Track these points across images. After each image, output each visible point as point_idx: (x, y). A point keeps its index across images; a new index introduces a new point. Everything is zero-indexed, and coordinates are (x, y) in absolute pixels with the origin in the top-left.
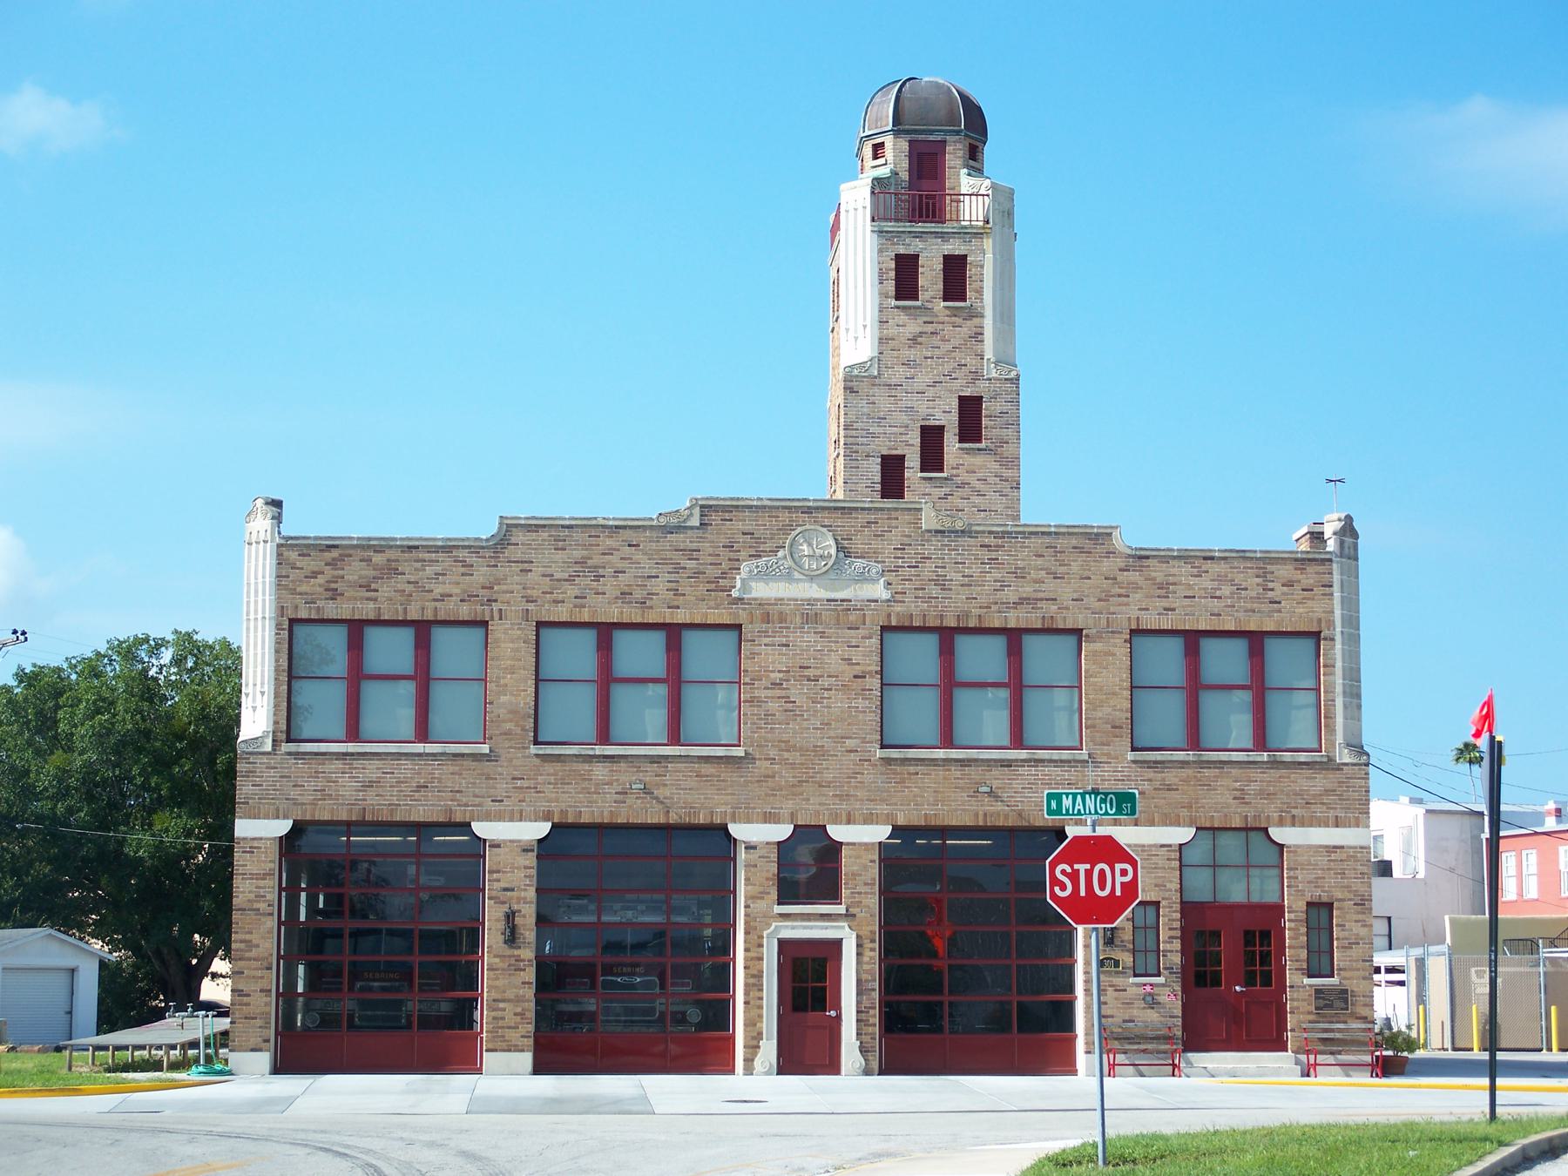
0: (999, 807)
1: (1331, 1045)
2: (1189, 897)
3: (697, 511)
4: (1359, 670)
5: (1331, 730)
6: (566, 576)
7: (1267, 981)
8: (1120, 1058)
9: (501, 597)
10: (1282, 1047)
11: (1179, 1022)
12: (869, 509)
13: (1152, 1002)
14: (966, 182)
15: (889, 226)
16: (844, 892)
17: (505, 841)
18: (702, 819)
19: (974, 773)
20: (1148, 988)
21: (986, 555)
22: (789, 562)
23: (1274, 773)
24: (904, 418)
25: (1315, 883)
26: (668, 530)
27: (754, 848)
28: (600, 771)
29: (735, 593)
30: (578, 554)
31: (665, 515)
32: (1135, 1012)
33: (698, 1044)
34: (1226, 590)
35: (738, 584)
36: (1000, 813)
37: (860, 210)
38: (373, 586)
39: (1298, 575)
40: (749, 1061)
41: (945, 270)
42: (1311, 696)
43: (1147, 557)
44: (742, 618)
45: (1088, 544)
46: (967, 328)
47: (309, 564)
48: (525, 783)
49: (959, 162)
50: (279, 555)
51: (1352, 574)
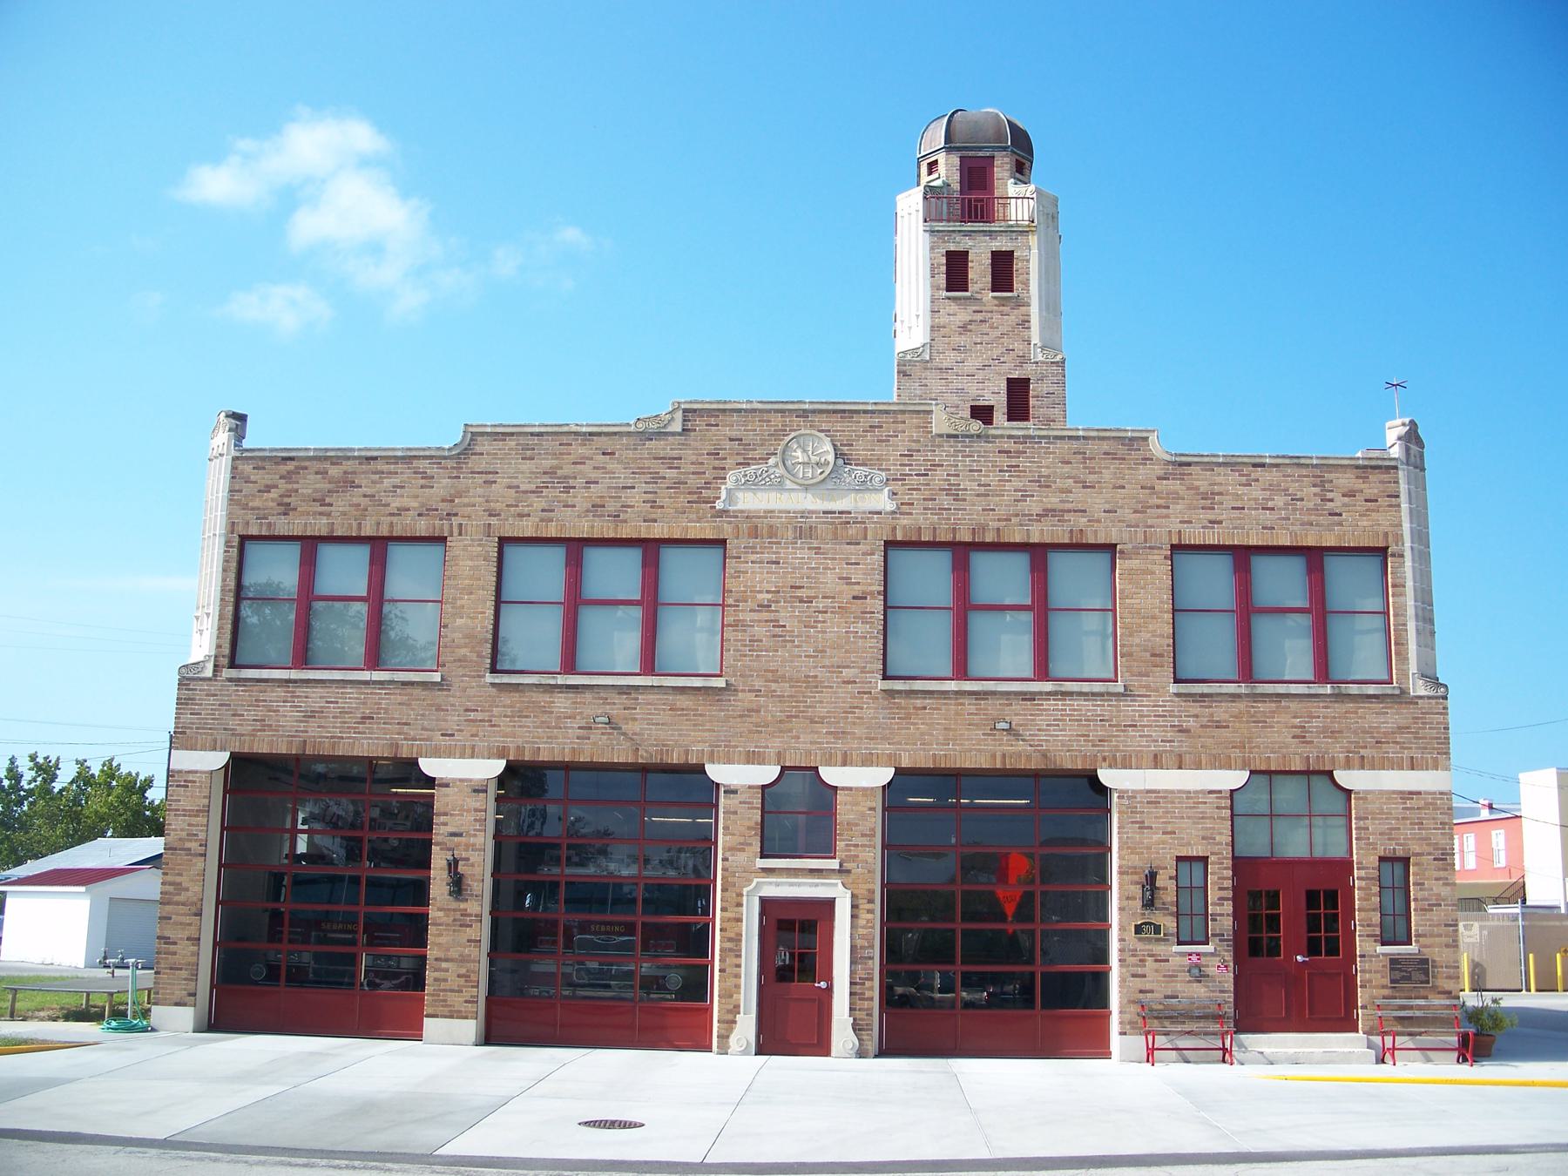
0: (1021, 746)
1: (1410, 1024)
2: (1244, 851)
3: (679, 415)
4: (1430, 592)
5: (1403, 658)
6: (533, 487)
7: (1333, 950)
8: (1161, 1041)
9: (461, 511)
10: (1354, 1028)
11: (1230, 997)
12: (873, 412)
13: (1200, 976)
14: (1012, 189)
15: (940, 226)
16: (840, 845)
17: (454, 780)
18: (675, 758)
19: (992, 707)
20: (1194, 958)
21: (1005, 461)
22: (781, 471)
23: (1340, 708)
24: (954, 399)
25: (1389, 834)
26: (646, 436)
27: (735, 792)
28: (562, 703)
29: (719, 505)
30: (548, 463)
31: (644, 420)
32: (1179, 986)
33: (666, 1013)
34: (1279, 501)
35: (723, 495)
36: (1020, 754)
37: (913, 217)
38: (328, 500)
39: (1359, 484)
40: (724, 1037)
41: (993, 264)
42: (1378, 621)
43: (1189, 464)
44: (727, 531)
45: (1121, 450)
46: (1014, 317)
47: (262, 478)
48: (479, 716)
49: (1007, 174)
50: (234, 468)
51: (1419, 485)
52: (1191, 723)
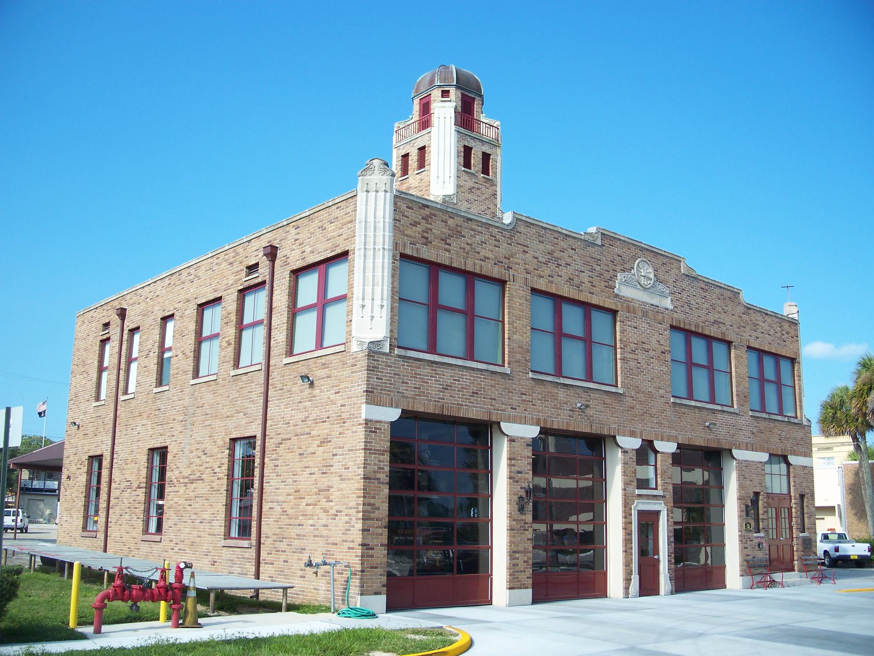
17: (517, 437)
27: (627, 452)
30: (550, 247)
37: (448, 119)
46: (490, 191)
50: (395, 204)
52: (755, 430)
